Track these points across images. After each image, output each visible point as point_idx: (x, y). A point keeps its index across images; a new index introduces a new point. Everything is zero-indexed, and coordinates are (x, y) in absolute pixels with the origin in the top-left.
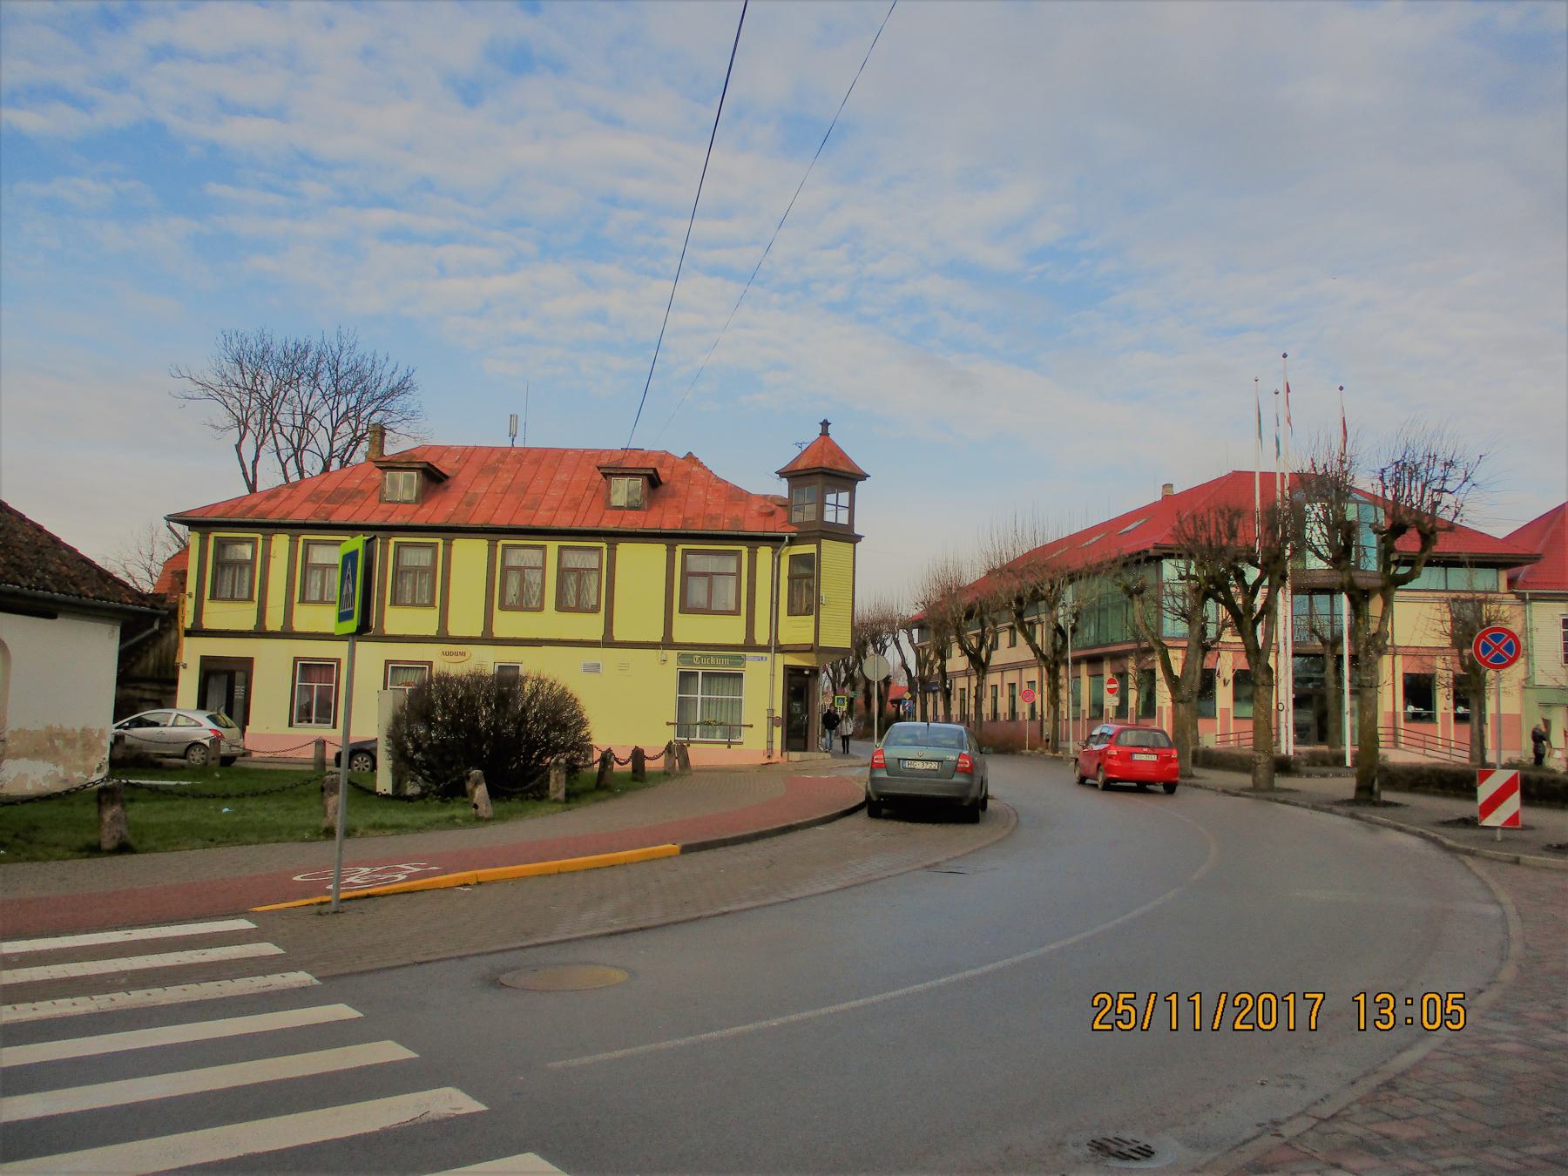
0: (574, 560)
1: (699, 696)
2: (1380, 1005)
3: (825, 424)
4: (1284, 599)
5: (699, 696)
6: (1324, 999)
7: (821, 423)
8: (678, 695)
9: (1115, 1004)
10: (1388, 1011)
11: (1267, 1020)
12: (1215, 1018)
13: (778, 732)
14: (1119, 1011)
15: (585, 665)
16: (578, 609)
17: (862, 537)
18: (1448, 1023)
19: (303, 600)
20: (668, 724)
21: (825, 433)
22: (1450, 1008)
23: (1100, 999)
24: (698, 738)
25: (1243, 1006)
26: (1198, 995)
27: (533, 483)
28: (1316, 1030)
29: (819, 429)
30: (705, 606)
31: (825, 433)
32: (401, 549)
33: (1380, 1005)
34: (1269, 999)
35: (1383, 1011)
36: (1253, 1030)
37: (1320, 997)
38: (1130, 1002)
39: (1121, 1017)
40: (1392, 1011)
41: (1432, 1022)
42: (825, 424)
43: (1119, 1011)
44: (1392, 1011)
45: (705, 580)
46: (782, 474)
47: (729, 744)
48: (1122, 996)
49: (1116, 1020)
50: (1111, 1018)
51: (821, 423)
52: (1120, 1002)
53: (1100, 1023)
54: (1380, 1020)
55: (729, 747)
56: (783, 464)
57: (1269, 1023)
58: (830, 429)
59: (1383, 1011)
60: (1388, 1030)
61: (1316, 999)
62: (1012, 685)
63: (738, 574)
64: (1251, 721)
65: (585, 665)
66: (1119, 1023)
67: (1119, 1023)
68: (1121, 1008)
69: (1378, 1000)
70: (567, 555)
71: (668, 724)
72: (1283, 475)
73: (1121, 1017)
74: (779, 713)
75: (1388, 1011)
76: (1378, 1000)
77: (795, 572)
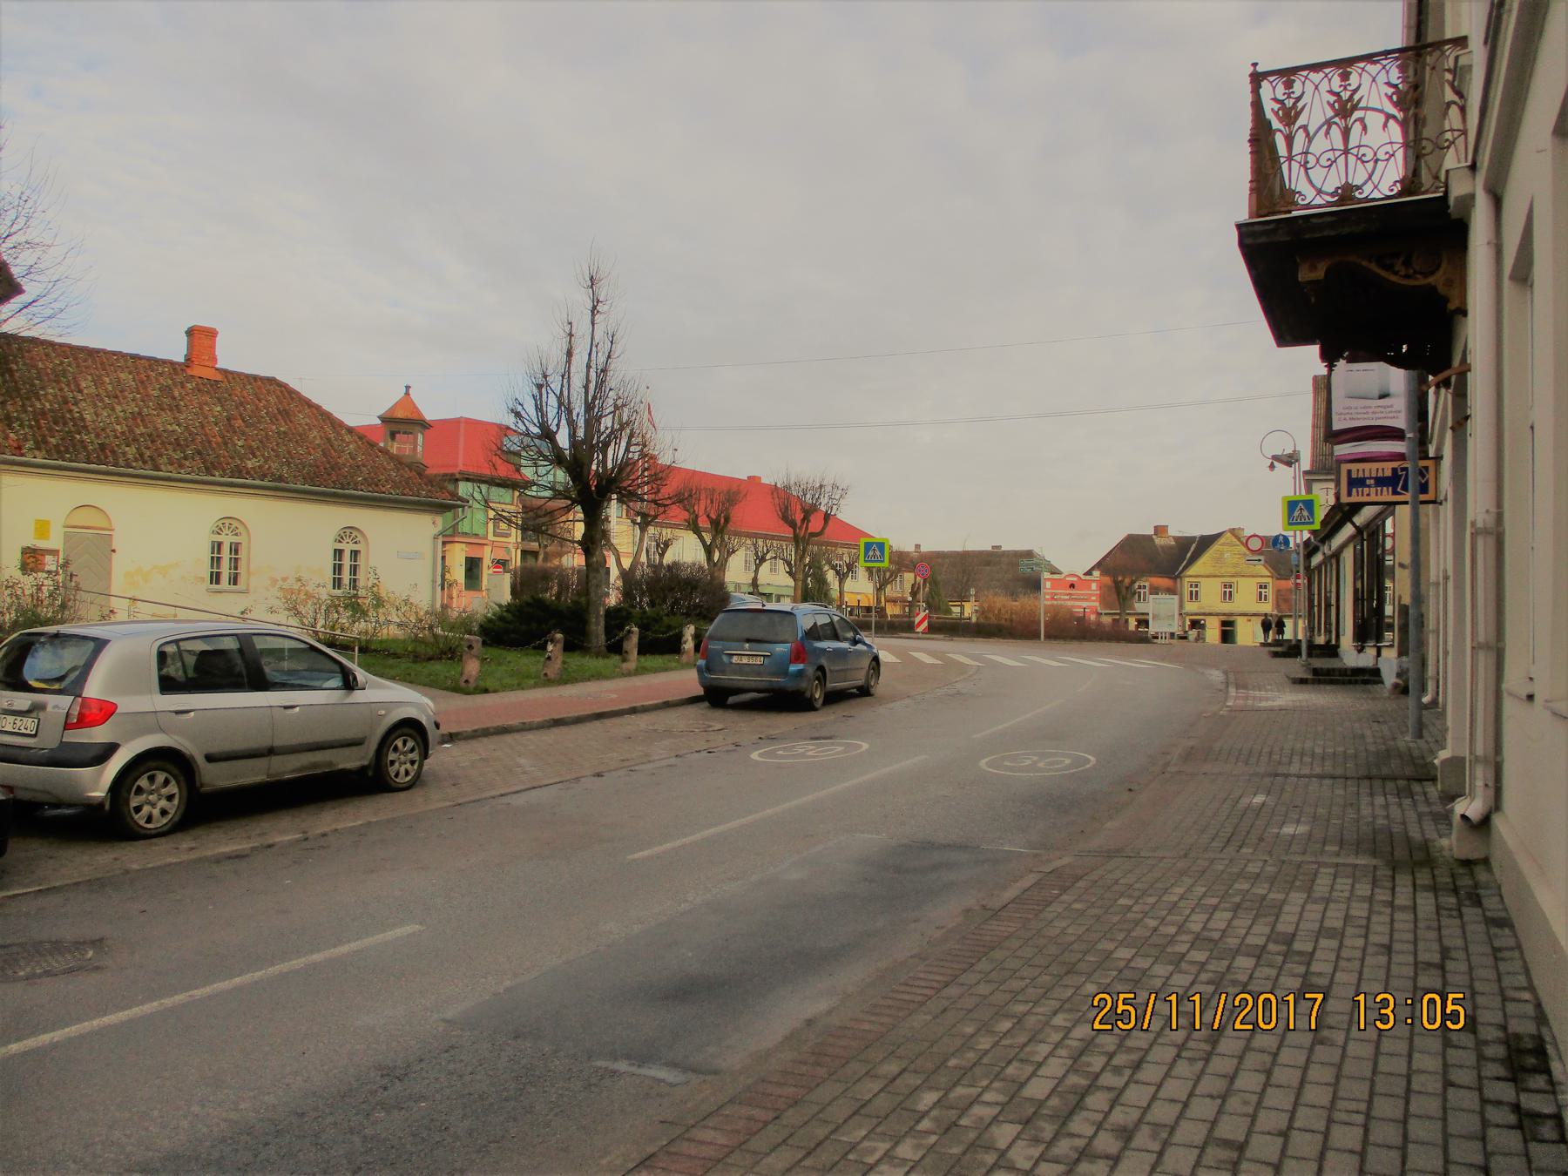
3: (408, 388)
6: (1324, 999)
10: (1388, 1011)
11: (1267, 1021)
14: (1119, 1011)
15: (211, 334)
17: (109, 641)
21: (407, 394)
22: (1450, 1008)
23: (1100, 999)
26: (1198, 995)
28: (1176, 1030)
31: (407, 394)
34: (1269, 999)
35: (1383, 1011)
36: (1112, 1030)
37: (1320, 997)
38: (1460, 1002)
39: (1120, 1017)
40: (1392, 1011)
42: (408, 388)
43: (1119, 1011)
44: (1392, 1011)
48: (1122, 996)
49: (1116, 1020)
52: (1120, 1002)
53: (1100, 1023)
57: (1269, 1023)
58: (411, 391)
59: (1383, 1011)
61: (1316, 999)
65: (211, 334)
66: (1119, 1023)
67: (1119, 1023)
68: (1121, 1008)
69: (1378, 1000)
73: (1120, 1017)
75: (1388, 1011)
76: (1378, 1000)
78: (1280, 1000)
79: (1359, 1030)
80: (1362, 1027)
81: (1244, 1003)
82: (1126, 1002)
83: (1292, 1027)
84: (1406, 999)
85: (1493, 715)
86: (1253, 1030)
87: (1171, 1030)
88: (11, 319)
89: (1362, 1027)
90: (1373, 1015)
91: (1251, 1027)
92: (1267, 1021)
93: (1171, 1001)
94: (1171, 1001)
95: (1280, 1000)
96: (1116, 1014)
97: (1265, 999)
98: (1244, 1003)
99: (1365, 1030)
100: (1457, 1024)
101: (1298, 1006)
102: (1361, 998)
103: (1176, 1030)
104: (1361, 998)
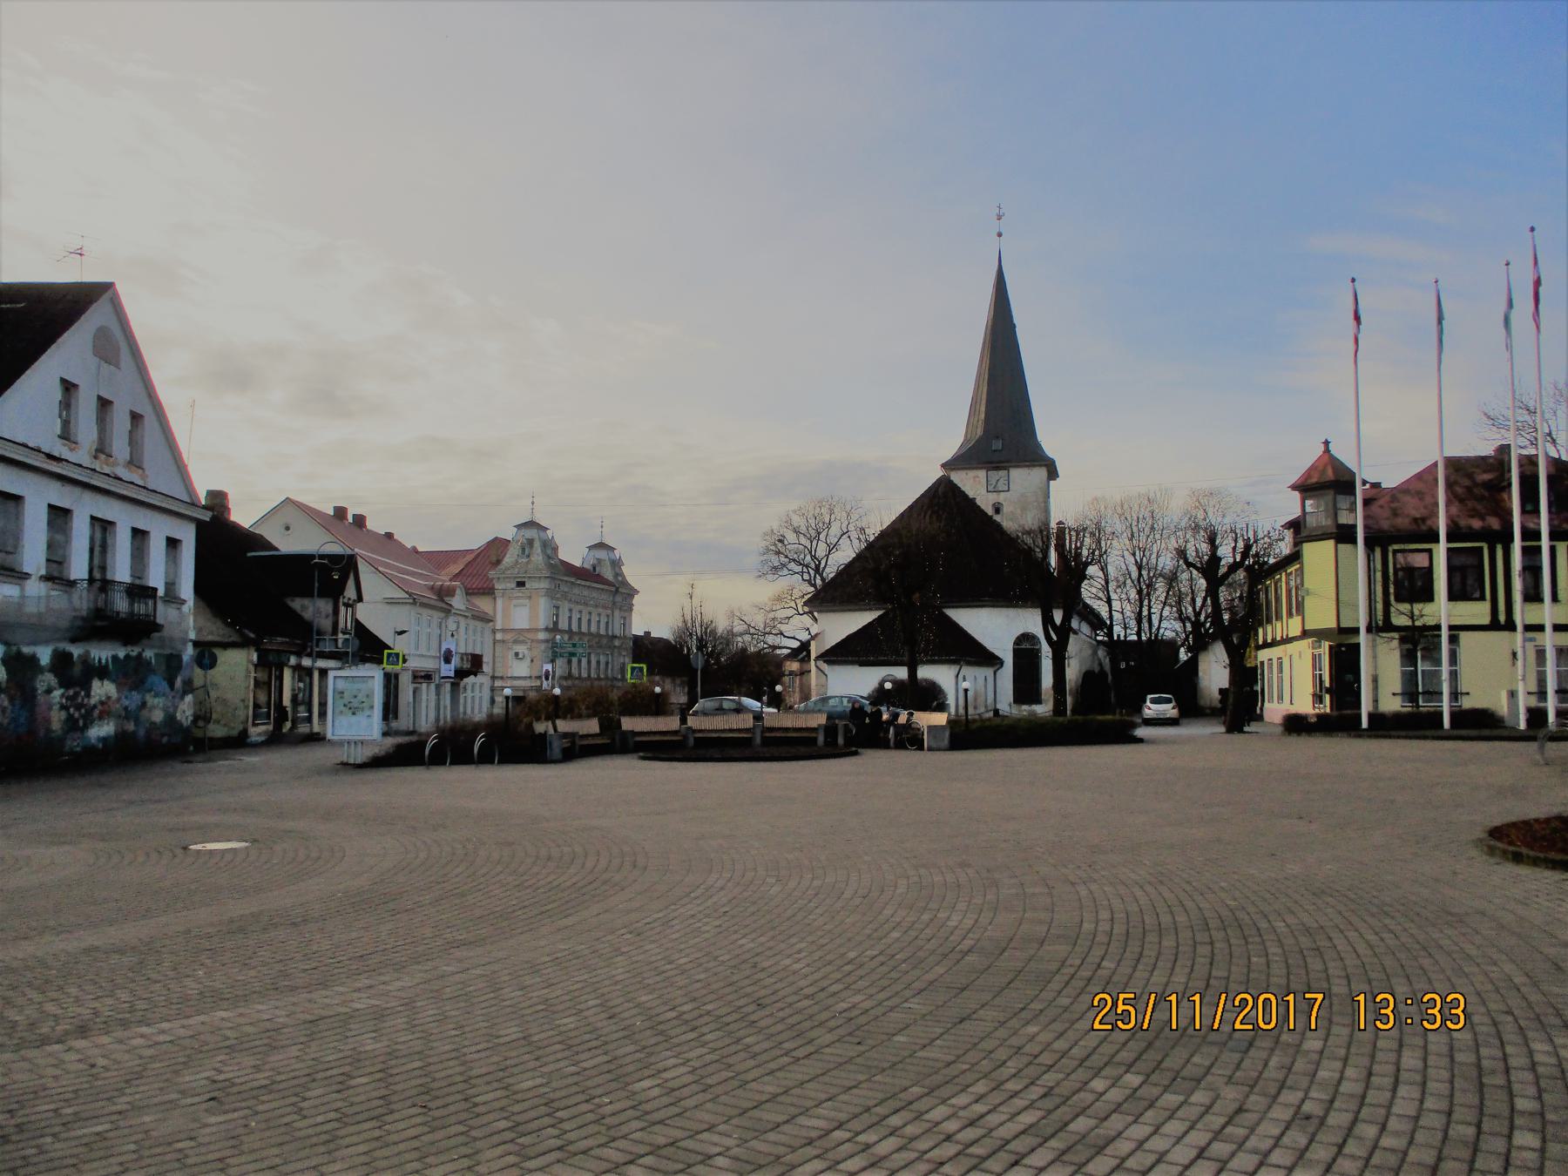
2: (1379, 1005)
3: (1326, 443)
4: (282, 643)
6: (1324, 999)
9: (1115, 1004)
11: (1267, 1020)
12: (1215, 1018)
14: (1119, 1011)
18: (1448, 1023)
21: (1327, 451)
23: (1101, 999)
25: (1101, 1006)
29: (1322, 448)
31: (1327, 451)
33: (1379, 1005)
39: (1121, 1017)
40: (1439, 1011)
41: (1267, 1021)
43: (1119, 1011)
44: (1439, 1011)
46: (1294, 487)
48: (1122, 996)
49: (1422, 1020)
50: (1110, 1019)
52: (1120, 1002)
53: (1100, 1023)
54: (1428, 1021)
56: (1294, 477)
57: (1269, 1023)
60: (1459, 1030)
61: (1316, 999)
62: (966, 691)
66: (1119, 1023)
67: (1119, 1023)
68: (1121, 1008)
72: (1529, 463)
73: (1121, 1017)
77: (1416, 573)
78: (1280, 1000)
79: (1171, 1030)
80: (1362, 1027)
81: (1103, 1002)
82: (1126, 1002)
83: (1216, 1027)
84: (1406, 999)
85: (1436, 742)
86: (1112, 1030)
87: (1310, 1030)
88: (1567, 543)
89: (1362, 1027)
90: (1371, 1017)
91: (1110, 1027)
92: (1267, 1020)
93: (1288, 1001)
94: (1288, 1001)
95: (1280, 1000)
96: (1116, 1014)
97: (1265, 999)
98: (1244, 1003)
99: (1365, 1030)
100: (1433, 1024)
101: (1181, 1005)
102: (1291, 998)
103: (1316, 1030)
104: (1291, 998)
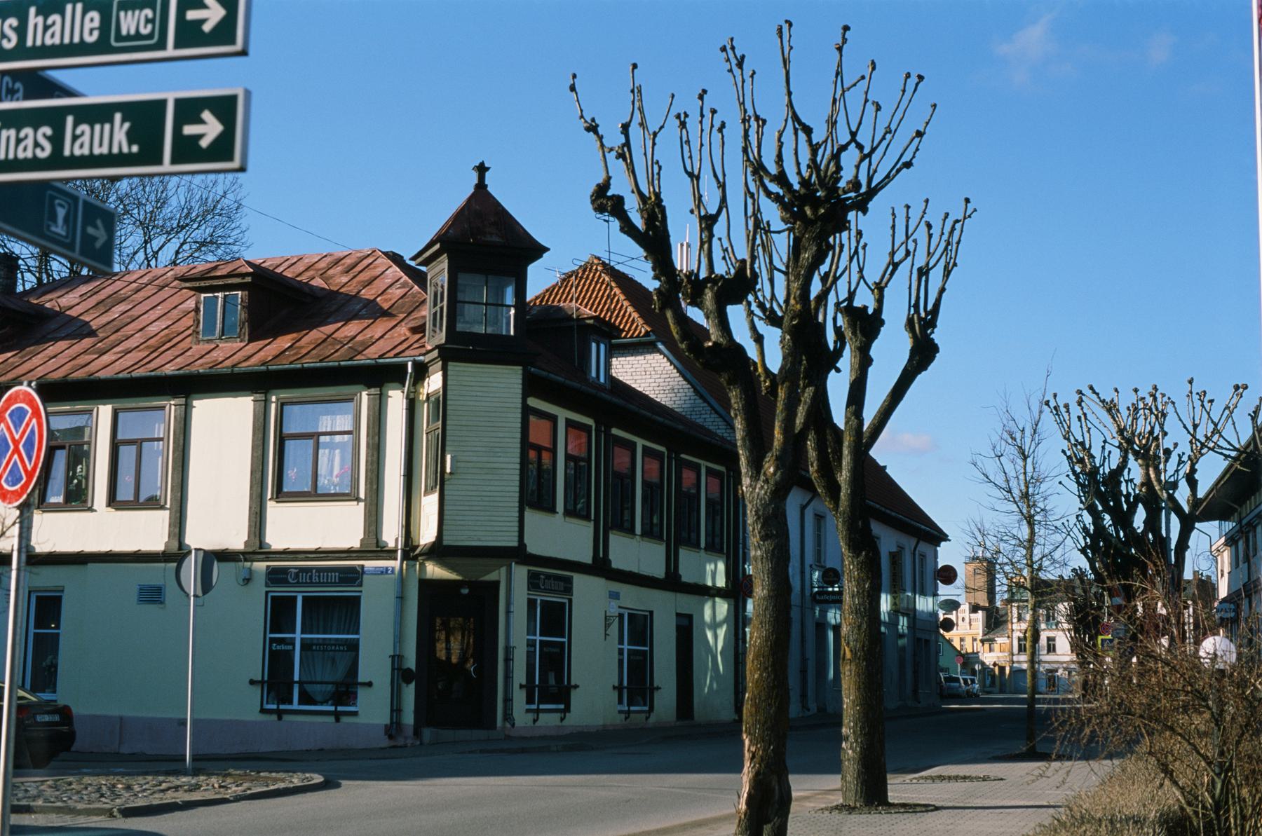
0: (133, 426)
1: (298, 636)
3: (482, 169)
5: (298, 636)
7: (488, 169)
8: (269, 636)
13: (409, 692)
16: (135, 504)
19: (281, 495)
20: (252, 682)
24: (295, 706)
27: (389, 291)
30: (285, 490)
32: (285, 407)
45: (134, 448)
47: (337, 716)
51: (488, 169)
55: (338, 720)
63: (354, 433)
64: (360, 680)
70: (293, 411)
71: (370, 684)
74: (411, 662)
